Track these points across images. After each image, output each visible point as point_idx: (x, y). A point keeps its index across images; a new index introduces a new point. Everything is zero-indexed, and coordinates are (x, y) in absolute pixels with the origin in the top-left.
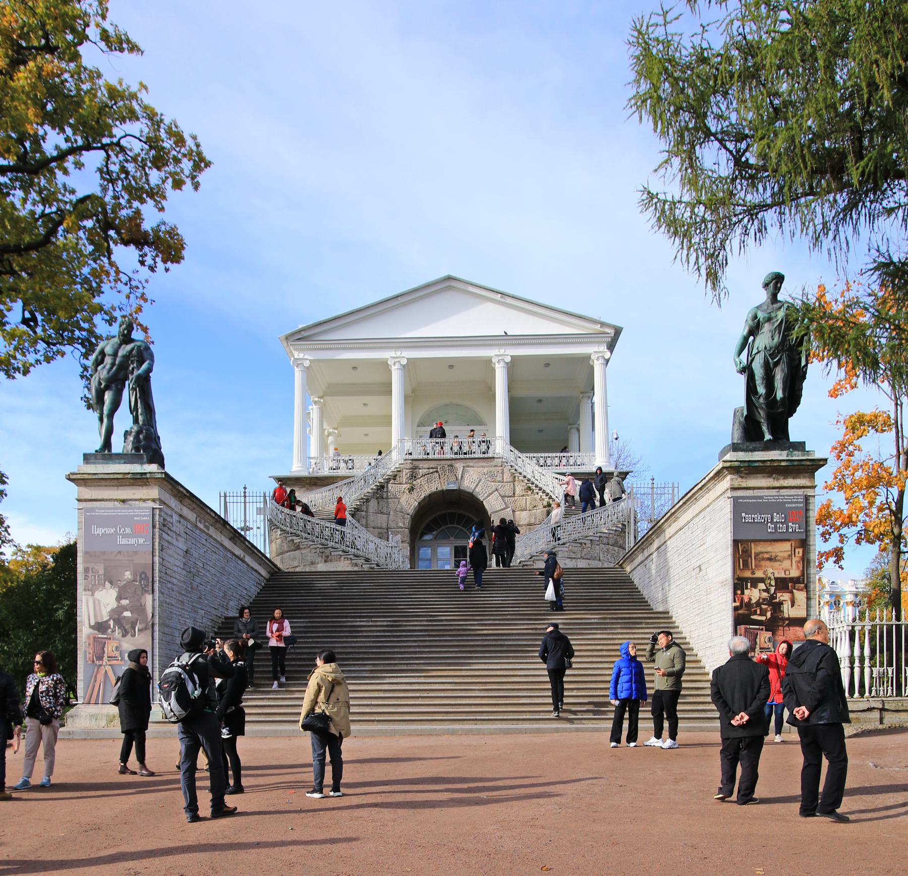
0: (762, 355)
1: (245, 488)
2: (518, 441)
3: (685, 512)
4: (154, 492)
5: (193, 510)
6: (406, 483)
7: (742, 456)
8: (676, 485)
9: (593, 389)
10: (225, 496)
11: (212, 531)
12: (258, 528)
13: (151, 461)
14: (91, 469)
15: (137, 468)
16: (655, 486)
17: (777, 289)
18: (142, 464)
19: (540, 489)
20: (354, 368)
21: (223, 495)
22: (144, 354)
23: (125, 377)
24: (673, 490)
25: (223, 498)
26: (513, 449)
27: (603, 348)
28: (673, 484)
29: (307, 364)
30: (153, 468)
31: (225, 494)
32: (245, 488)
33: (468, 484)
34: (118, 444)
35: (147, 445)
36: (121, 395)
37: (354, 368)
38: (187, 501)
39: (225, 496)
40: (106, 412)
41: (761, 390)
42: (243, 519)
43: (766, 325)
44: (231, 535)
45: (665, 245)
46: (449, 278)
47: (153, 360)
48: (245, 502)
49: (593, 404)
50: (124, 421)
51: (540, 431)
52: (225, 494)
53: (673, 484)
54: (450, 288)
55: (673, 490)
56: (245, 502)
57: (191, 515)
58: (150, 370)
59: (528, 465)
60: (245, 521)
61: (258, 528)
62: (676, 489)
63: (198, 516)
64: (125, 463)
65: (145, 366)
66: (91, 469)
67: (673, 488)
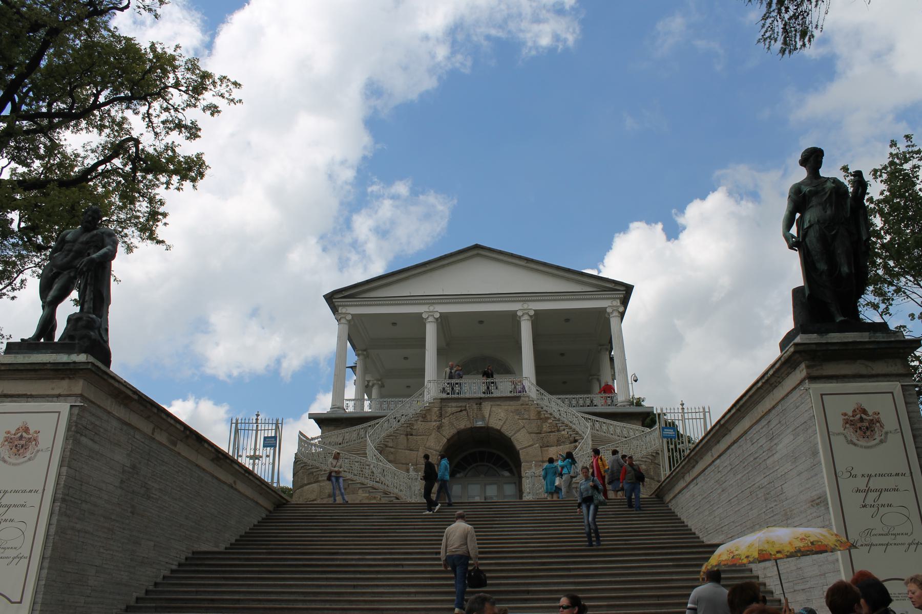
0: (817, 227)
2: (541, 382)
4: (78, 386)
5: (148, 418)
6: (435, 421)
7: (813, 338)
8: (707, 410)
9: (611, 342)
12: (268, 456)
16: (686, 411)
17: (818, 164)
19: (567, 426)
20: (394, 324)
21: (234, 421)
24: (705, 415)
25: (234, 425)
26: (539, 388)
27: (617, 303)
28: (704, 409)
29: (349, 317)
31: (237, 420)
33: (495, 423)
37: (394, 324)
39: (237, 424)
41: (822, 266)
42: (253, 447)
43: (814, 198)
46: (477, 247)
49: (612, 359)
50: (67, 308)
51: (564, 383)
52: (237, 420)
53: (704, 409)
54: (478, 255)
55: (705, 415)
56: (257, 430)
57: (146, 427)
59: (555, 405)
60: (255, 449)
61: (268, 456)
62: (707, 414)
64: (52, 353)
67: (704, 412)
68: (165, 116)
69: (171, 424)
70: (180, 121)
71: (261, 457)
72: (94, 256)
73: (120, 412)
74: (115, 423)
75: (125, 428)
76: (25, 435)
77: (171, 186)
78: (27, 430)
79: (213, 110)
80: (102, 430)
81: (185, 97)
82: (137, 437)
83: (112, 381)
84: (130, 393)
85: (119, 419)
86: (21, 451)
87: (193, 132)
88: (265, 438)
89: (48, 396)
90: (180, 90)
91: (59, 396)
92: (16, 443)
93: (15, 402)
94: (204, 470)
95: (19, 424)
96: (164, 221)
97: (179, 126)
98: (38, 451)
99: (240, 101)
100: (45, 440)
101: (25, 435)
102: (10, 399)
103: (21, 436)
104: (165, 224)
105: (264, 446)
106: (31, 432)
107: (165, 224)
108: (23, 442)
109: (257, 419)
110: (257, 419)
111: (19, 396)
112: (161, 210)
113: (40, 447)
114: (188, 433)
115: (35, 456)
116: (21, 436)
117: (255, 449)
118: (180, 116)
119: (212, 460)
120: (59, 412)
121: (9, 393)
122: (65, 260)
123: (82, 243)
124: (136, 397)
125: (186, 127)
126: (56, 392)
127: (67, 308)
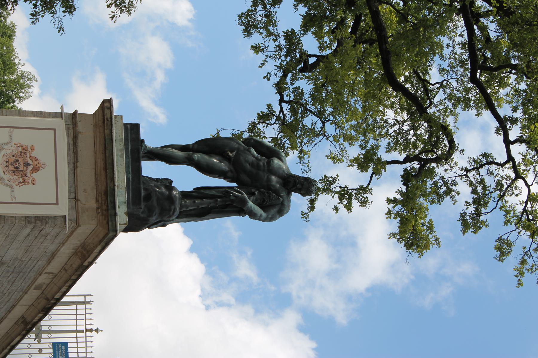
1: (97, 330)
3: (69, 145)
5: (64, 269)
10: (85, 303)
11: (33, 294)
13: (130, 215)
14: (118, 134)
15: (121, 196)
16: (89, 334)
18: (128, 203)
21: (88, 299)
22: (272, 204)
23: (247, 180)
25: (82, 299)
30: (122, 217)
31: (89, 303)
32: (97, 330)
34: (151, 169)
35: (154, 207)
36: (219, 177)
38: (77, 262)
39: (85, 303)
40: (197, 156)
42: (54, 328)
44: (29, 319)
45: (480, 232)
47: (265, 220)
48: (76, 331)
50: (186, 179)
52: (89, 303)
56: (76, 331)
57: (55, 266)
58: (253, 215)
60: (50, 332)
61: (40, 350)
63: (55, 276)
65: (258, 210)
66: (118, 134)
68: (490, 182)
69: (60, 288)
70: (486, 204)
71: (39, 342)
72: (251, 204)
73: (66, 251)
74: (52, 248)
75: (48, 254)
76: (30, 168)
77: (392, 205)
78: (36, 169)
79: (503, 247)
80: (41, 240)
81: (519, 208)
82: (40, 263)
83: (99, 248)
84: (90, 260)
85: (57, 250)
86: (11, 168)
87: (471, 223)
88: (65, 345)
89: (76, 186)
90: (526, 203)
91: (76, 199)
92: (21, 160)
93: (69, 149)
94: (9, 311)
95: (42, 159)
96: (341, 207)
97: (479, 202)
98: (11, 187)
99: (520, 284)
100: (24, 193)
101: (30, 168)
102: (71, 143)
103: (28, 165)
104: (336, 209)
105: (54, 344)
106: (34, 175)
107: (336, 209)
108: (21, 167)
109: (91, 330)
110: (91, 330)
111: (76, 153)
112: (355, 203)
113: (16, 188)
114: (53, 301)
115: (6, 185)
116: (28, 165)
117: (50, 332)
118: (491, 205)
119: (23, 317)
120: (57, 204)
121: (79, 141)
122: (248, 166)
123: (269, 180)
124: (86, 264)
125: (478, 213)
126: (81, 196)
127: (186, 179)
